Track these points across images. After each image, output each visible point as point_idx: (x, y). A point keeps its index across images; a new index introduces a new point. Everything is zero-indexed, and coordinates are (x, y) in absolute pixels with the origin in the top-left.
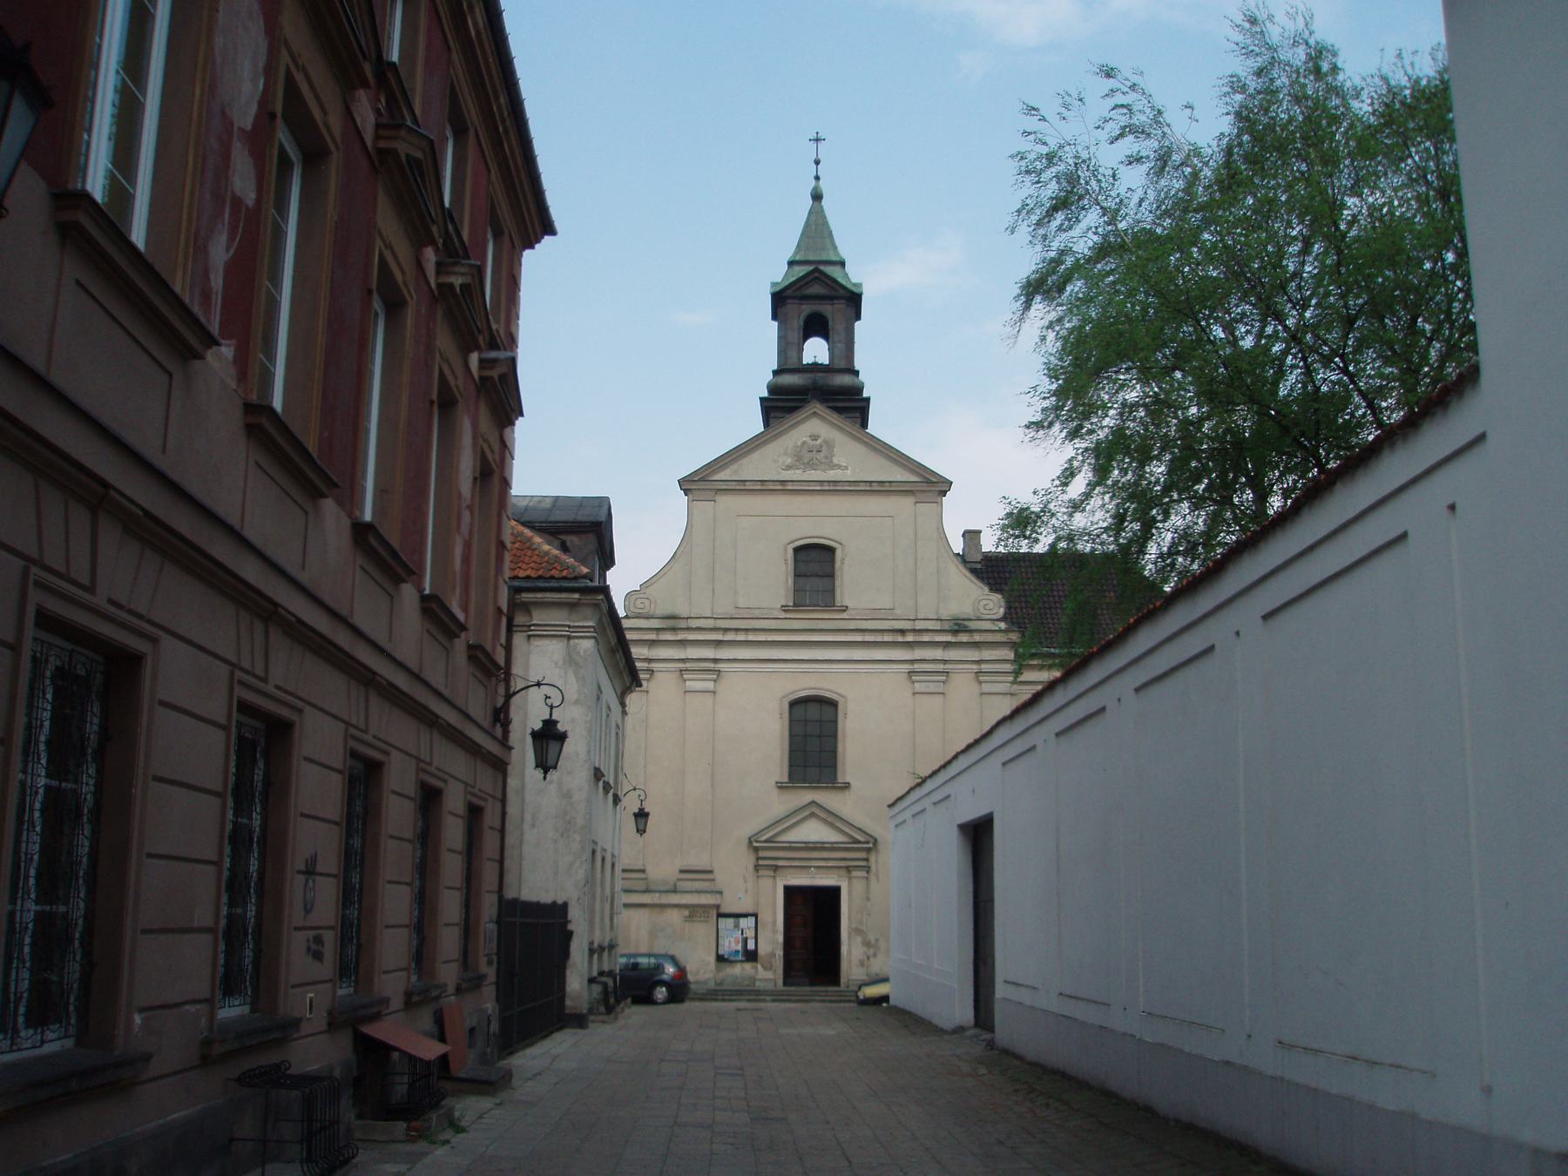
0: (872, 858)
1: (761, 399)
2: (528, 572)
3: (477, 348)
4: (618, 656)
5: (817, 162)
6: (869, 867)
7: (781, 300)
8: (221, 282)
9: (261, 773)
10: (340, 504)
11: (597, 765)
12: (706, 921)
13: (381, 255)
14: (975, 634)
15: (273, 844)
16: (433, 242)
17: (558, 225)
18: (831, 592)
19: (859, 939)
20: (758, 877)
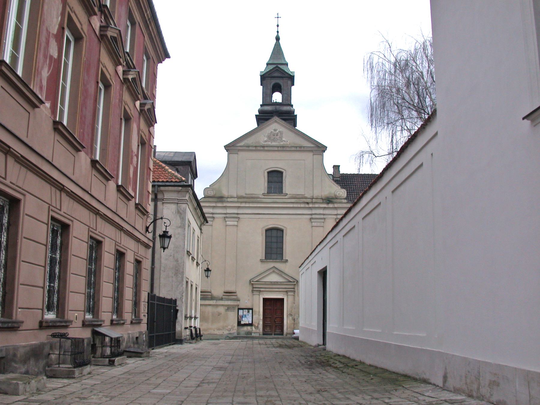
0: (296, 288)
1: (256, 115)
2: (163, 180)
3: (139, 99)
4: (197, 211)
5: (278, 26)
6: (295, 291)
7: (264, 78)
8: (46, 84)
9: (60, 241)
10: (87, 153)
11: (188, 250)
12: (234, 311)
13: (102, 70)
14: (335, 204)
15: (64, 264)
16: (121, 64)
17: (171, 55)
18: (281, 188)
19: (291, 318)
20: (253, 295)
